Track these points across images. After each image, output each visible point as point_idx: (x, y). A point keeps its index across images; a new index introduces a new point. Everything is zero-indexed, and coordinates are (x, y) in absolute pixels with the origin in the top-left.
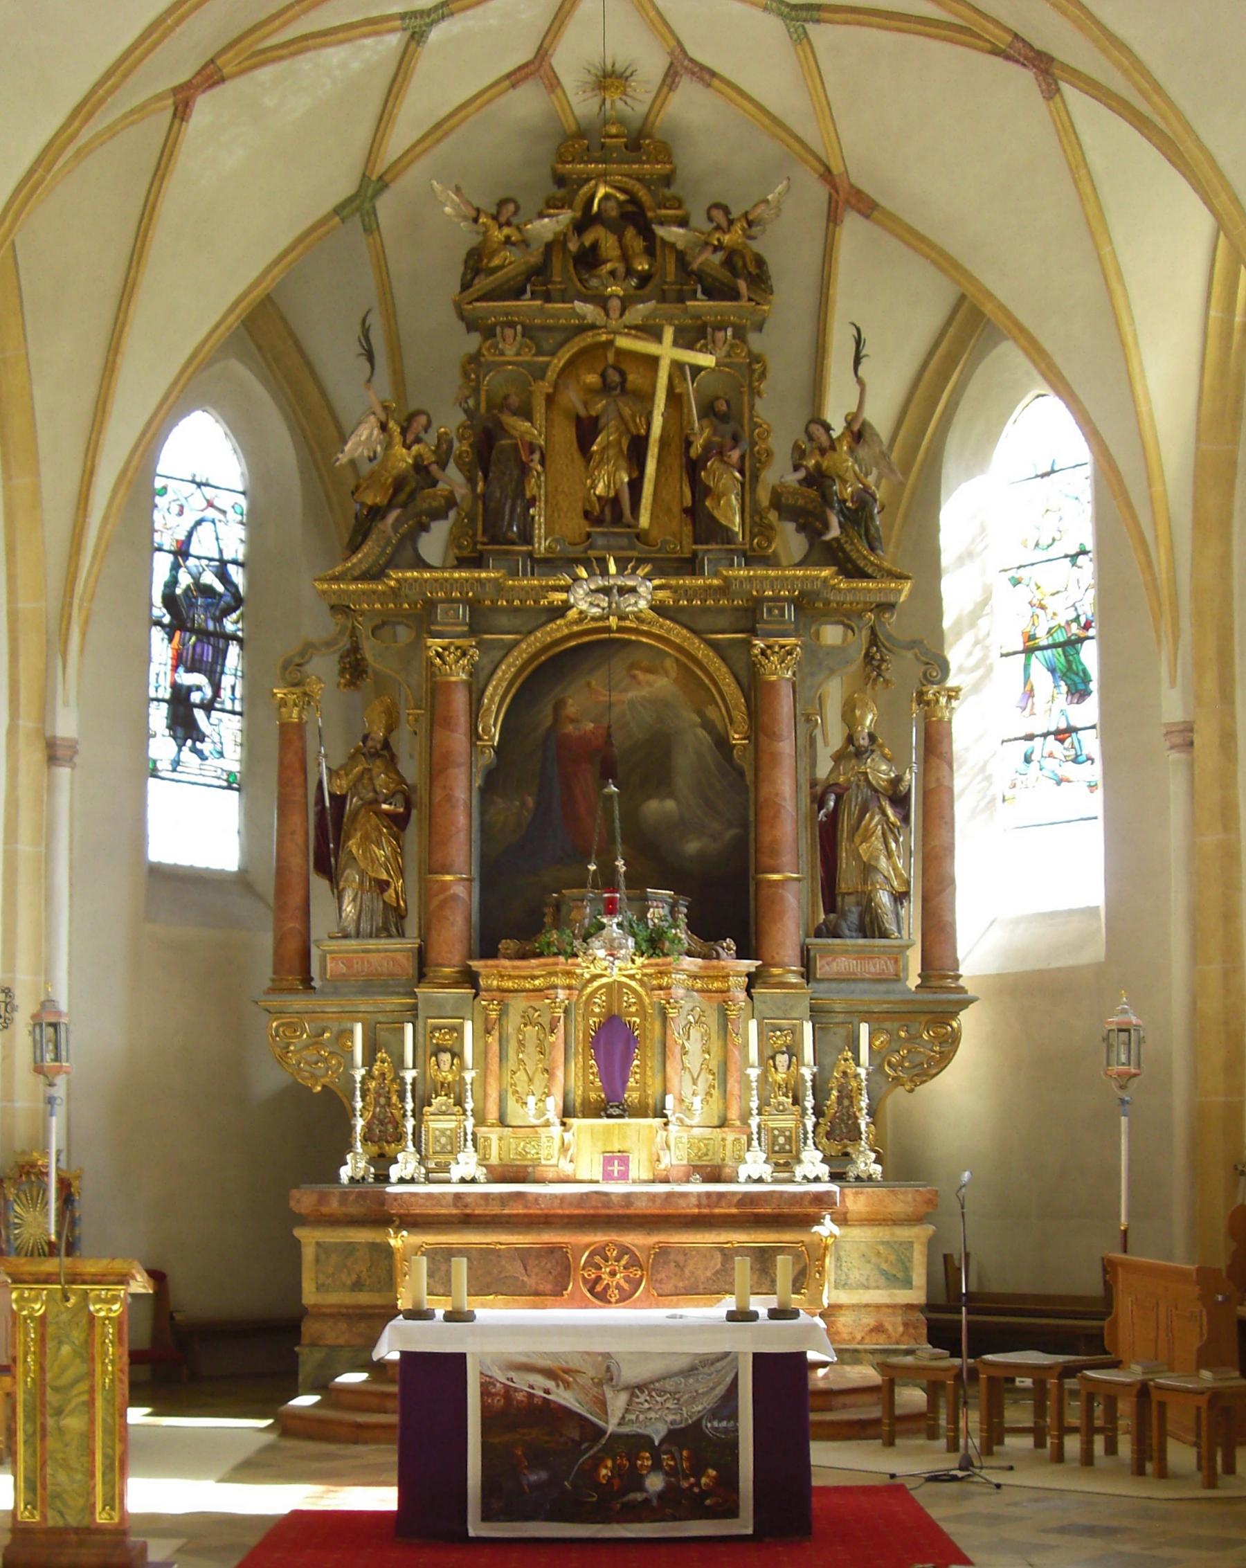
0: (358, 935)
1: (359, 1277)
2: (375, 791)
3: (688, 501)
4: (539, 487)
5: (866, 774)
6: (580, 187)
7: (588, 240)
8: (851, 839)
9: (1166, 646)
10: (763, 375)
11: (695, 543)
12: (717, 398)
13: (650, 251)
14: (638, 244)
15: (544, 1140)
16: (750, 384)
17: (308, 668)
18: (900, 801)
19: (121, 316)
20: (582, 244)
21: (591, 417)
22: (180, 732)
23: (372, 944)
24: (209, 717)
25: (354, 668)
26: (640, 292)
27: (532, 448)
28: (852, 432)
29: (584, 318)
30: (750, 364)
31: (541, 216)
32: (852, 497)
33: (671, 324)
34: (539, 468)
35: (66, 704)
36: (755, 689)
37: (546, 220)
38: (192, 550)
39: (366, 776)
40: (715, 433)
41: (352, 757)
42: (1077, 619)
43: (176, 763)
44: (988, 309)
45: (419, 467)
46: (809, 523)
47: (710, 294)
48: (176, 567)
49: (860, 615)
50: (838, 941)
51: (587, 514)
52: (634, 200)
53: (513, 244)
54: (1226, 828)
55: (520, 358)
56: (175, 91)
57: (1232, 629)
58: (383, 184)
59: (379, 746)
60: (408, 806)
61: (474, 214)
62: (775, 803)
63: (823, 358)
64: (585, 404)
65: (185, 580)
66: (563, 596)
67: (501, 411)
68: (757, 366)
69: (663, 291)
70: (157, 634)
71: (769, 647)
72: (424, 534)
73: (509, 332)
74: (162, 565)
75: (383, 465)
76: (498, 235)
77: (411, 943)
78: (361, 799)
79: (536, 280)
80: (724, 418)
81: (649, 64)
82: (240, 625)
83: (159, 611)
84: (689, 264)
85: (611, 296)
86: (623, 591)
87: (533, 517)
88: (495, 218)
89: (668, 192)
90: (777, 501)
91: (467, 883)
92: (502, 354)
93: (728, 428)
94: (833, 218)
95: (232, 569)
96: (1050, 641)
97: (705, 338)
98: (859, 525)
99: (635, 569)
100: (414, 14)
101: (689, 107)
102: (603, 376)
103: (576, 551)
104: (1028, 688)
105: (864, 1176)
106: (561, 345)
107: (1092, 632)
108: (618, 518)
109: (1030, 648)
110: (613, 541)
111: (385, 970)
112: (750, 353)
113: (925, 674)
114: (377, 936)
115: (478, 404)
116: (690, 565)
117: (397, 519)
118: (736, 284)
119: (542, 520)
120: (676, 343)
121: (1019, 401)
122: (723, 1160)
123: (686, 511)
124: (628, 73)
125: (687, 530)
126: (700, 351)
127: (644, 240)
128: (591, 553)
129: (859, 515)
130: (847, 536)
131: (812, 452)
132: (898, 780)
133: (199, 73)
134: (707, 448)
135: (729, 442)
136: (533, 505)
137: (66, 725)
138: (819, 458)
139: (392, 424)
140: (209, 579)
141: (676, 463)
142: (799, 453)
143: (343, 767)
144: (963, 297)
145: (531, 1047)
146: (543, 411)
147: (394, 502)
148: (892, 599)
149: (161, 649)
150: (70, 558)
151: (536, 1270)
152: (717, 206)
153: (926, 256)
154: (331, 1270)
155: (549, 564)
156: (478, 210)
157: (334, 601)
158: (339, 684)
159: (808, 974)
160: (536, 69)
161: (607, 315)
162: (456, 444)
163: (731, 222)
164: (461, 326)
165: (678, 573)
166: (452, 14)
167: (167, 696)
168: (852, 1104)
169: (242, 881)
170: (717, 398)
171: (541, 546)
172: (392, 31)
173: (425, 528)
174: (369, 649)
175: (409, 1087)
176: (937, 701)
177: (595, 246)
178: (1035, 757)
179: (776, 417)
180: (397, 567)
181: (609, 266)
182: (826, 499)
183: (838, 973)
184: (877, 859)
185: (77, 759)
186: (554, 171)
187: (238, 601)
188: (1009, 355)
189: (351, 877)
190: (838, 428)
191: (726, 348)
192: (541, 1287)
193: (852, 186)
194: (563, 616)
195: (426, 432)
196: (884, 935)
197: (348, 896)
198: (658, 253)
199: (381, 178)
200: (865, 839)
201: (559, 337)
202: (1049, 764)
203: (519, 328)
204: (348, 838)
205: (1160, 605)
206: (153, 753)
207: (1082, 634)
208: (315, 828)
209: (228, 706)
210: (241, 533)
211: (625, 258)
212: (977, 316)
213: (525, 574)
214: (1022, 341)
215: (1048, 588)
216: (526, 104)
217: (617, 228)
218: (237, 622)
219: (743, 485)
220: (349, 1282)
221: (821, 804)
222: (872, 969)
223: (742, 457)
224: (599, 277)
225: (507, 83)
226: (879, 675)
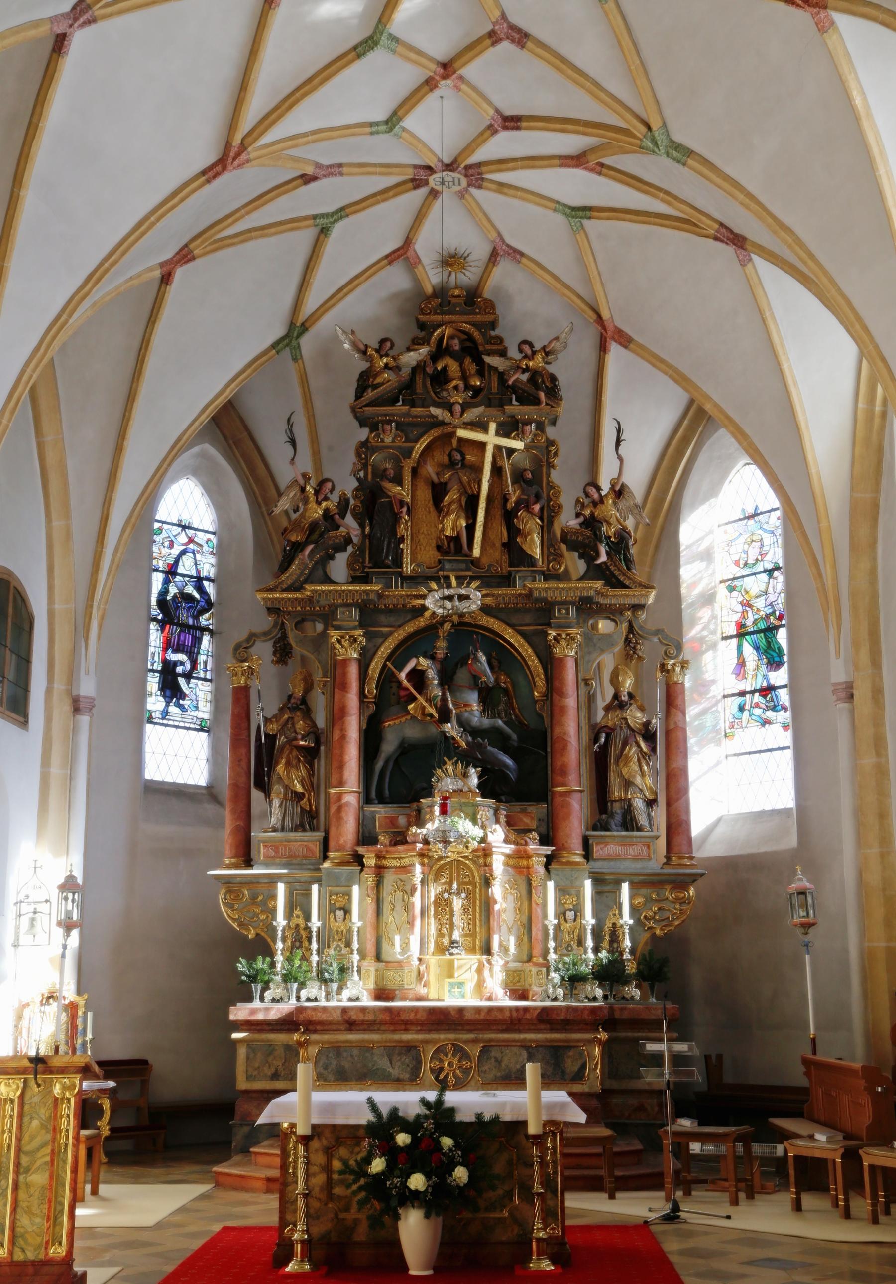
0: (283, 830)
1: (276, 1070)
2: (296, 732)
3: (505, 538)
4: (407, 530)
5: (626, 719)
8: (617, 763)
9: (832, 631)
10: (556, 454)
11: (510, 566)
13: (481, 373)
14: (473, 368)
15: (406, 971)
16: (548, 459)
17: (252, 650)
18: (649, 736)
19: (127, 414)
20: (436, 368)
21: (441, 483)
22: (168, 692)
23: (292, 834)
24: (188, 683)
25: (283, 652)
27: (402, 503)
28: (615, 491)
29: (436, 417)
30: (547, 447)
31: (409, 350)
32: (615, 534)
33: (494, 421)
34: (406, 517)
35: (87, 673)
36: (551, 665)
37: (412, 353)
38: (179, 571)
39: (290, 723)
40: (523, 492)
41: (281, 710)
42: (774, 612)
43: (165, 713)
44: (708, 407)
45: (327, 514)
46: (588, 552)
47: (522, 401)
48: (166, 582)
49: (621, 614)
50: (608, 833)
51: (439, 548)
52: (470, 338)
53: (390, 369)
54: (878, 754)
55: (394, 444)
56: (162, 265)
57: (878, 619)
58: (304, 328)
59: (299, 702)
60: (318, 743)
62: (564, 739)
63: (598, 442)
64: (438, 474)
65: (173, 590)
66: (418, 602)
67: (381, 480)
69: (489, 399)
70: (153, 626)
73: (388, 427)
74: (158, 579)
75: (303, 516)
77: (320, 835)
78: (286, 737)
79: (407, 391)
80: (529, 483)
81: (479, 251)
82: (211, 622)
83: (155, 611)
84: (507, 381)
85: (454, 403)
86: (462, 598)
87: (402, 550)
88: (377, 351)
89: (493, 333)
90: (564, 539)
91: (357, 794)
92: (382, 441)
93: (535, 488)
94: (603, 348)
95: (206, 584)
96: (755, 628)
97: (517, 430)
98: (620, 553)
99: (469, 584)
100: (322, 216)
101: (505, 280)
102: (450, 455)
103: (431, 572)
104: (741, 661)
105: (628, 996)
106: (421, 436)
107: (784, 622)
108: (459, 549)
109: (742, 633)
110: (455, 565)
111: (301, 854)
112: (547, 439)
113: (665, 653)
114: (296, 831)
116: (507, 581)
117: (312, 551)
120: (498, 434)
121: (733, 468)
122: (530, 985)
123: (504, 545)
124: (466, 254)
125: (505, 558)
126: (514, 439)
128: (441, 573)
130: (612, 560)
131: (588, 505)
132: (647, 724)
133: (177, 253)
134: (518, 503)
135: (532, 498)
136: (403, 542)
137: (87, 687)
139: (308, 488)
140: (190, 590)
141: (498, 513)
143: (275, 716)
144: (692, 402)
145: (399, 906)
148: (642, 602)
149: (155, 637)
150: (92, 575)
151: (399, 1064)
152: (525, 342)
153: (666, 373)
154: (257, 1065)
155: (414, 580)
156: (366, 346)
157: (269, 605)
158: (273, 661)
159: (588, 855)
160: (402, 254)
161: (452, 415)
162: (352, 502)
163: (534, 353)
164: (357, 424)
165: (499, 586)
166: (348, 216)
167: (160, 668)
168: (619, 946)
169: (210, 793)
170: (525, 470)
171: (408, 568)
172: (307, 227)
173: (332, 557)
174: (292, 637)
175: (314, 934)
176: (674, 670)
177: (445, 369)
178: (747, 707)
180: (312, 583)
181: (454, 383)
182: (598, 537)
183: (609, 855)
184: (634, 777)
185: (94, 710)
186: (417, 320)
187: (209, 605)
188: (722, 440)
189: (277, 789)
190: (605, 488)
192: (402, 1076)
193: (616, 327)
194: (422, 615)
196: (639, 829)
197: (276, 803)
199: (303, 324)
200: (626, 764)
202: (757, 712)
204: (277, 763)
205: (828, 602)
206: (149, 706)
207: (777, 623)
208: (258, 756)
209: (202, 675)
210: (212, 560)
211: (465, 378)
212: (701, 413)
213: (397, 587)
214: (732, 429)
215: (754, 592)
216: (397, 280)
217: (458, 357)
218: (208, 620)
219: (542, 527)
220: (269, 1074)
221: (596, 740)
222: (632, 852)
223: (542, 509)
224: (447, 390)
225: (386, 261)
226: (634, 653)
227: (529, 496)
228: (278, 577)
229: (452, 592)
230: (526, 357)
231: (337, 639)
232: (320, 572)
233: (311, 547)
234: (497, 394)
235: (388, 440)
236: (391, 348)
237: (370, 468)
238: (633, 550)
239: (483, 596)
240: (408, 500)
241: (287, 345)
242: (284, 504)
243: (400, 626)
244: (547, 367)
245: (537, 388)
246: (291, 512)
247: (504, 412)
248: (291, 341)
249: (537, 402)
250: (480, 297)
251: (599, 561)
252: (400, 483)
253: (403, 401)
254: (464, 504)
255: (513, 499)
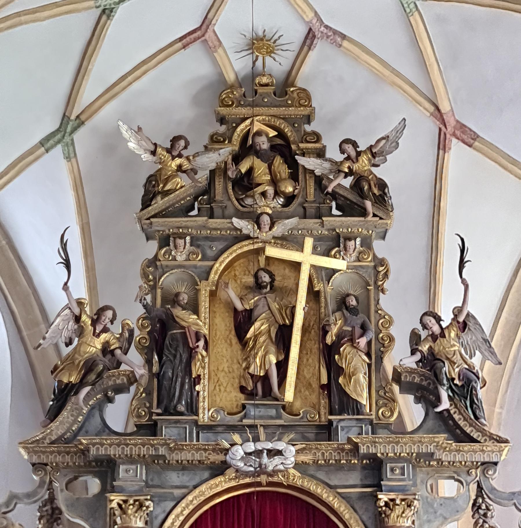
3: (324, 380)
4: (204, 368)
6: (238, 125)
7: (244, 168)
10: (386, 275)
11: (331, 414)
12: (348, 295)
13: (294, 177)
21: (246, 310)
26: (286, 209)
27: (198, 336)
28: (458, 322)
30: (375, 267)
34: (204, 353)
40: (346, 322)
45: (106, 350)
46: (427, 396)
51: (243, 389)
52: (281, 134)
53: (184, 172)
58: (80, 122)
61: (152, 148)
67: (173, 307)
68: (381, 269)
71: (393, 500)
72: (109, 405)
73: (180, 242)
76: (174, 164)
79: (204, 199)
80: (353, 311)
81: (292, 34)
85: (262, 214)
86: (273, 453)
87: (198, 392)
89: (308, 128)
90: (397, 377)
92: (174, 259)
93: (358, 320)
94: (442, 146)
97: (339, 246)
102: (256, 276)
103: (234, 420)
108: (268, 392)
110: (263, 411)
115: (154, 299)
118: (364, 204)
119: (206, 394)
124: (276, 37)
125: (324, 402)
127: (289, 168)
129: (466, 390)
130: (456, 407)
134: (340, 336)
135: (358, 331)
138: (432, 344)
139: (84, 318)
141: (314, 346)
142: (415, 339)
146: (207, 305)
147: (85, 381)
152: (347, 141)
160: (199, 35)
161: (259, 228)
162: (137, 332)
163: (359, 154)
170: (348, 295)
171: (204, 416)
179: (399, 309)
181: (260, 189)
186: (217, 114)
190: (447, 319)
191: (354, 255)
195: (112, 323)
198: (301, 177)
199: (78, 117)
201: (217, 246)
203: (188, 238)
211: (274, 182)
216: (193, 66)
219: (369, 365)
223: (369, 343)
224: (253, 197)
227: (353, 327)
228: (45, 426)
229: (260, 446)
230: (348, 158)
231: (119, 505)
232: (96, 420)
233: (87, 389)
234: (314, 202)
235: (181, 258)
236: (186, 147)
237: (159, 291)
238: (481, 393)
239: (298, 452)
240: (205, 331)
241: (59, 142)
242: (328, 201)
243: (195, 487)
244: (374, 170)
245: (363, 195)
246: (62, 346)
247: (322, 224)
248: (63, 137)
249: (363, 213)
250: (293, 85)
251: (439, 409)
252: (196, 311)
253: (199, 209)
254: (273, 336)
255: (334, 330)
